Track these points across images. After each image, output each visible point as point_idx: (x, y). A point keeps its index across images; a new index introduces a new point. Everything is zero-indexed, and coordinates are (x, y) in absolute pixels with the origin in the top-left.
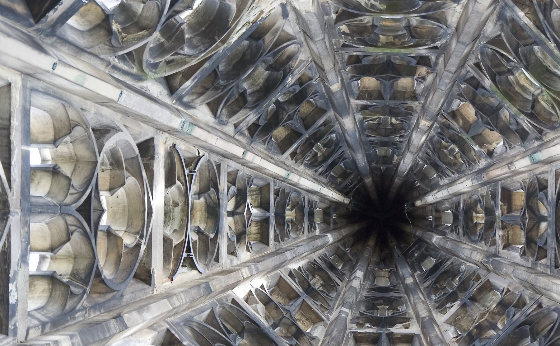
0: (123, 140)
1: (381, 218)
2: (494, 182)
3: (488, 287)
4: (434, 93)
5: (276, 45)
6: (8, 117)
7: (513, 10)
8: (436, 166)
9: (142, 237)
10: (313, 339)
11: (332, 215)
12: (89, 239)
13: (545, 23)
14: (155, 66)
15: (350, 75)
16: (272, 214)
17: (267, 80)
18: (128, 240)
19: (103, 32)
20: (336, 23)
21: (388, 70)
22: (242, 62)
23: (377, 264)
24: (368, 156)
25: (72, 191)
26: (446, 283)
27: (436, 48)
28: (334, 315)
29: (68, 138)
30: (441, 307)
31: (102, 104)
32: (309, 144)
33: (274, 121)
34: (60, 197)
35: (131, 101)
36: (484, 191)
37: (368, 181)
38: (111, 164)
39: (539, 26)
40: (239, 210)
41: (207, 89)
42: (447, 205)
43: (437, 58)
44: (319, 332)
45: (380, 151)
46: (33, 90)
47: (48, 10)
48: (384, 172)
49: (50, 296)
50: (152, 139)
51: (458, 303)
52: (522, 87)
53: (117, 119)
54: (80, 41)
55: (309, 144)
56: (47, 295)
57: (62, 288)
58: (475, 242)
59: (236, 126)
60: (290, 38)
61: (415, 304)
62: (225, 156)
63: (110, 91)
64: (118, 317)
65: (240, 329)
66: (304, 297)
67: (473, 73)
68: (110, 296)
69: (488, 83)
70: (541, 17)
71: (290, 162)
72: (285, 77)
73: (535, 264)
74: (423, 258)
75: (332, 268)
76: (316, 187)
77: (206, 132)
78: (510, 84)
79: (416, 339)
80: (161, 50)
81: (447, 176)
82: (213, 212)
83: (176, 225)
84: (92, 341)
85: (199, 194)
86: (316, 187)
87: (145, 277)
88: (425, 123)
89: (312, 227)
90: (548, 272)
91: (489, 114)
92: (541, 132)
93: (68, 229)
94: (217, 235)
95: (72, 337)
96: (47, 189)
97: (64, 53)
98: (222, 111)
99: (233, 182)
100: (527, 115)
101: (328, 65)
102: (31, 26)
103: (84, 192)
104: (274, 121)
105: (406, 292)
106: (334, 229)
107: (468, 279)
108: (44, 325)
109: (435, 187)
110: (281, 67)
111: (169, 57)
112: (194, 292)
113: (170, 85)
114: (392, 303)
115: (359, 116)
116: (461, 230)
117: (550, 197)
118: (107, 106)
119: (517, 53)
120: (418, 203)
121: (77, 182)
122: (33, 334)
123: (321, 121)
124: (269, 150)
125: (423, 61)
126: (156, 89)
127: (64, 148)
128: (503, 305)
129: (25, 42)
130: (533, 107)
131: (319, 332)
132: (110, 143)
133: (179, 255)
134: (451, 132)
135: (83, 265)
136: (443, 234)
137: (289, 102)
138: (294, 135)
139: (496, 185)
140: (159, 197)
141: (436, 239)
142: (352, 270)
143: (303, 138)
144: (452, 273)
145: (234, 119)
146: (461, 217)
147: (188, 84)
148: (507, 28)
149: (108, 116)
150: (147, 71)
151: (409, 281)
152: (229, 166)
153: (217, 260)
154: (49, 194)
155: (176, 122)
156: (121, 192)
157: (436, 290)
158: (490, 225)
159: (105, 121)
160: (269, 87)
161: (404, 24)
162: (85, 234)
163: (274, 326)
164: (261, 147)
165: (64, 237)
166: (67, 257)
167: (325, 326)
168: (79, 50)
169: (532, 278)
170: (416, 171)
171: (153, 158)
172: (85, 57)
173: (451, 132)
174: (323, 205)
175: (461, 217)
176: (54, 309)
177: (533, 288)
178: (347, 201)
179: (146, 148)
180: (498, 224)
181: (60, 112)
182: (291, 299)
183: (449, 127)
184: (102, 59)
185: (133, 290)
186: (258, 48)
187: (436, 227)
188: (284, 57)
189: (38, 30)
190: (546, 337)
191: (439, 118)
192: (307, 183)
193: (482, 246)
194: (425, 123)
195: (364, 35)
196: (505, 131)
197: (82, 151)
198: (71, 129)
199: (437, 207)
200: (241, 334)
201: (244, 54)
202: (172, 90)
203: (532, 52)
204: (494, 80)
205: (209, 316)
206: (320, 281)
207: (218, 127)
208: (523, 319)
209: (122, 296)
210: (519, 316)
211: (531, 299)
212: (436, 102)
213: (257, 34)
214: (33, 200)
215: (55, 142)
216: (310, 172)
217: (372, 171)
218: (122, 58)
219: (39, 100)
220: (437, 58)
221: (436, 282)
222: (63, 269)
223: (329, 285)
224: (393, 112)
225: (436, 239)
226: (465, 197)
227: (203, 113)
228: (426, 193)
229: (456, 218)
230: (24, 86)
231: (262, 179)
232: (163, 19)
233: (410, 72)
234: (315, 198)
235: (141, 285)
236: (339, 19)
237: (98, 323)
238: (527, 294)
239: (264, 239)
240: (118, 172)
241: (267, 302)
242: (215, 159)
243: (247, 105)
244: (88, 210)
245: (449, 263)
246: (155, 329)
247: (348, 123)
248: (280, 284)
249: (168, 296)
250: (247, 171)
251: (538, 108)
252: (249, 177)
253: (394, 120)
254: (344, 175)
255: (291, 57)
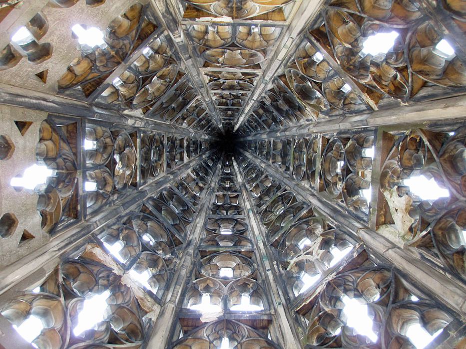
0: (261, 59)
1: (227, 144)
2: (241, 192)
3: (201, 189)
4: (273, 170)
5: (296, 115)
6: (272, 19)
7: (306, 209)
8: (247, 167)
9: (222, 64)
10: (182, 124)
11: (229, 126)
12: (222, 46)
13: (302, 221)
14: (290, 72)
15: (283, 140)
16: (230, 107)
17: (282, 110)
18: (221, 59)
19: (304, 55)
20: (304, 138)
21: (284, 155)
22: (289, 102)
23: (210, 142)
24: (251, 141)
25: (241, 41)
26: (203, 172)
27: (293, 175)
28: (191, 130)
29: (262, 39)
30: (194, 170)
31: (275, 52)
32: (256, 121)
33: (266, 111)
34: (238, 36)
35: (276, 64)
36: (237, 186)
37: (242, 140)
38: (251, 54)
39: (300, 219)
40: (232, 96)
41: (279, 89)
42: (232, 170)
43: (288, 174)
44: (185, 125)
45: (253, 145)
46: (283, 28)
47: (315, 37)
48: (246, 146)
49: (198, 31)
50: (261, 69)
51: (196, 177)
52: (277, 207)
53: (270, 57)
54: (301, 46)
55: (256, 121)
56: (199, 30)
57: (202, 37)
58: (218, 183)
59: (264, 97)
60: (298, 120)
61: (195, 160)
62: (253, 93)
63: (281, 56)
64: (190, 57)
65: (185, 98)
66: (198, 119)
67: (283, 188)
68: (199, 53)
69: (279, 194)
70: (304, 220)
71: (250, 114)
72: (283, 117)
73: (210, 209)
74: (213, 160)
75: (209, 127)
76: (240, 122)
77: (261, 89)
78: (278, 202)
79: (182, 162)
80: (297, 74)
81: (243, 171)
82: (232, 87)
83: (226, 75)
84: (181, 48)
85: (238, 83)
86: (240, 122)
87: (206, 65)
88: (263, 165)
89: (224, 120)
90: (207, 215)
91: (267, 192)
92: (260, 213)
93: (226, 39)
94: (222, 89)
95: (182, 42)
96: (242, 31)
97: (297, 41)
98: (270, 93)
99: (242, 95)
100: (266, 208)
101: (287, 133)
102: (309, 30)
103: (241, 45)
104: (266, 111)
105: (200, 155)
106: (224, 127)
107: (204, 181)
108: (187, 30)
109: (239, 165)
110: (287, 115)
111: (293, 78)
112: (200, 83)
113: (282, 76)
114: (195, 151)
115: (267, 140)
116: (222, 176)
117: (235, 216)
118: (275, 54)
119: (291, 207)
120: (233, 158)
121: (245, 43)
122: (184, 27)
123: (265, 126)
124: (255, 107)
125: (288, 169)
126: (280, 71)
127: (258, 37)
128: (194, 197)
129: (302, 28)
130: (269, 211)
131: (185, 125)
132: (259, 54)
133: (214, 77)
134: (260, 175)
135: (211, 44)
136: (222, 168)
137: (273, 116)
138: (260, 116)
139: (240, 192)
140: (239, 71)
141: (220, 166)
142: (208, 134)
143: (259, 120)
144: (207, 174)
145: (267, 97)
146: (227, 176)
147: (282, 83)
148: (299, 205)
149: (270, 55)
150: (288, 69)
151: (204, 157)
152: (249, 94)
153: (212, 89)
154: (240, 32)
155: (267, 78)
156: (240, 57)
157: (200, 167)
158: (225, 189)
159: (268, 53)
160: (279, 110)
161: (302, 163)
162: (223, 45)
163: (187, 110)
164: (256, 105)
165: (222, 38)
166: (214, 37)
167: (187, 127)
168: (298, 46)
169: (205, 209)
170: (245, 159)
171: (253, 68)
172: (295, 48)
173: (260, 175)
174: (233, 123)
175: (227, 176)
176: (194, 34)
177: (201, 210)
178: (234, 131)
179: (258, 66)
180: (225, 193)
181: (273, 37)
182: (197, 114)
183: (262, 174)
184: (293, 54)
185: (201, 61)
186: (295, 109)
187: (224, 165)
188: (290, 117)
189: (306, 32)
190: (183, 217)
191: (265, 171)
192: (241, 119)
193: (217, 186)
194: (263, 165)
195: (299, 148)
196: (260, 198)
197: (257, 44)
198: (266, 41)
199: (231, 165)
200: (183, 99)
201: (293, 103)
202: (280, 77)
203: (291, 214)
204: (280, 196)
205: (191, 87)
206: (205, 123)
207: (264, 91)
208: (189, 206)
209: (199, 57)
210: (190, 204)
211: (197, 208)
212: (271, 171)
213: (300, 109)
214: (238, 27)
215: (261, 34)
216: (245, 120)
217: (246, 142)
218: (294, 60)
219: (278, 30)
220: (288, 174)
221: (203, 167)
222: (210, 36)
223: (202, 127)
224: (268, 153)
225: (220, 166)
226: (235, 178)
227: (270, 86)
228: (237, 162)
229: (227, 174)
230: (284, 25)
231: (244, 104)
232: (309, 78)
233: (284, 163)
234: (235, 121)
235: (203, 63)
236: (306, 140)
237: (188, 50)
238: (199, 207)
239: (220, 104)
240: (248, 56)
241: (196, 107)
242: (252, 89)
243: (273, 102)
244: (233, 46)
245: (211, 172)
246: (185, 69)
247: (264, 137)
248: (203, 110)
249: (199, 74)
250: (247, 100)
251: (269, 213)
252: (244, 100)
253: (265, 152)
254: (244, 131)
255: (290, 119)
